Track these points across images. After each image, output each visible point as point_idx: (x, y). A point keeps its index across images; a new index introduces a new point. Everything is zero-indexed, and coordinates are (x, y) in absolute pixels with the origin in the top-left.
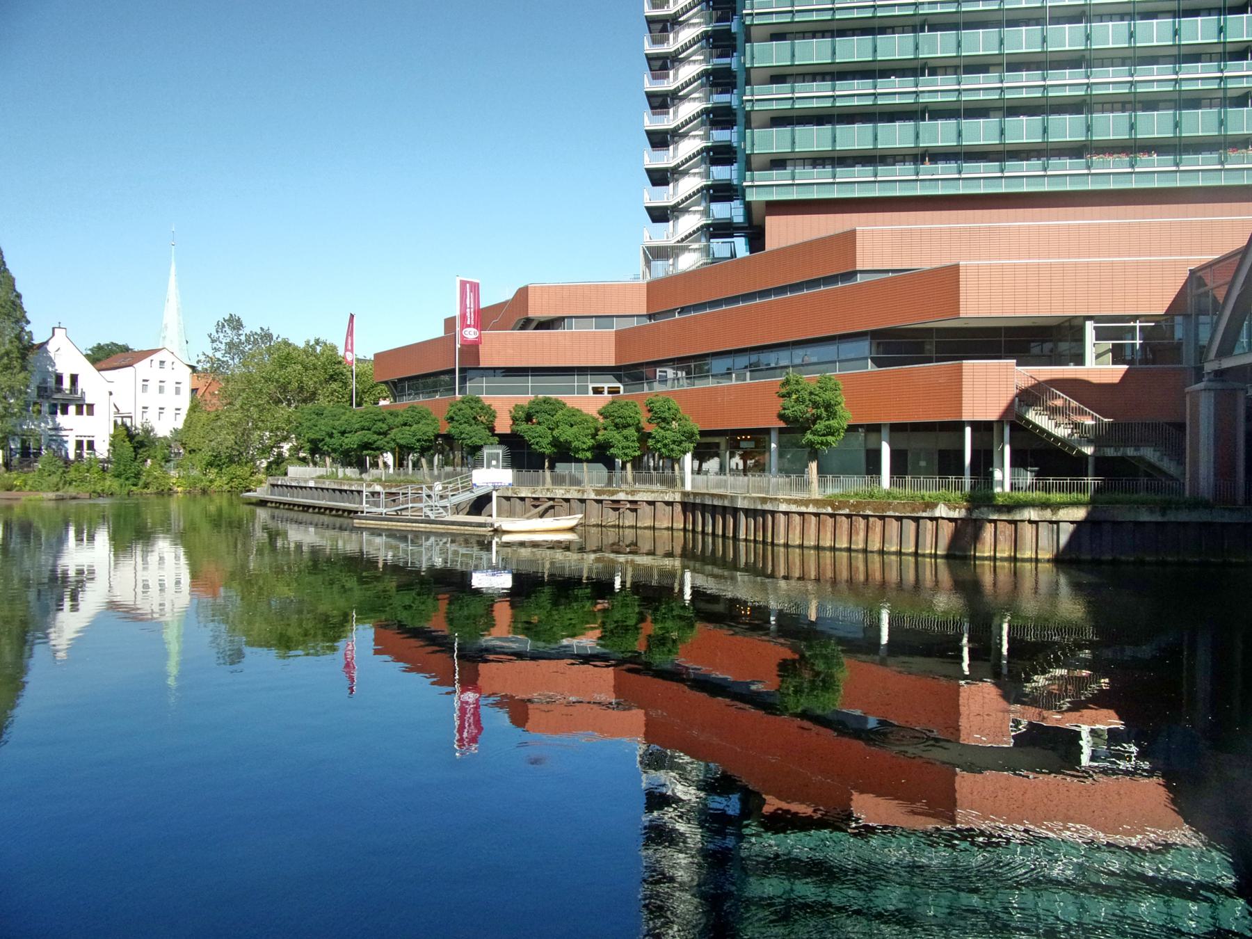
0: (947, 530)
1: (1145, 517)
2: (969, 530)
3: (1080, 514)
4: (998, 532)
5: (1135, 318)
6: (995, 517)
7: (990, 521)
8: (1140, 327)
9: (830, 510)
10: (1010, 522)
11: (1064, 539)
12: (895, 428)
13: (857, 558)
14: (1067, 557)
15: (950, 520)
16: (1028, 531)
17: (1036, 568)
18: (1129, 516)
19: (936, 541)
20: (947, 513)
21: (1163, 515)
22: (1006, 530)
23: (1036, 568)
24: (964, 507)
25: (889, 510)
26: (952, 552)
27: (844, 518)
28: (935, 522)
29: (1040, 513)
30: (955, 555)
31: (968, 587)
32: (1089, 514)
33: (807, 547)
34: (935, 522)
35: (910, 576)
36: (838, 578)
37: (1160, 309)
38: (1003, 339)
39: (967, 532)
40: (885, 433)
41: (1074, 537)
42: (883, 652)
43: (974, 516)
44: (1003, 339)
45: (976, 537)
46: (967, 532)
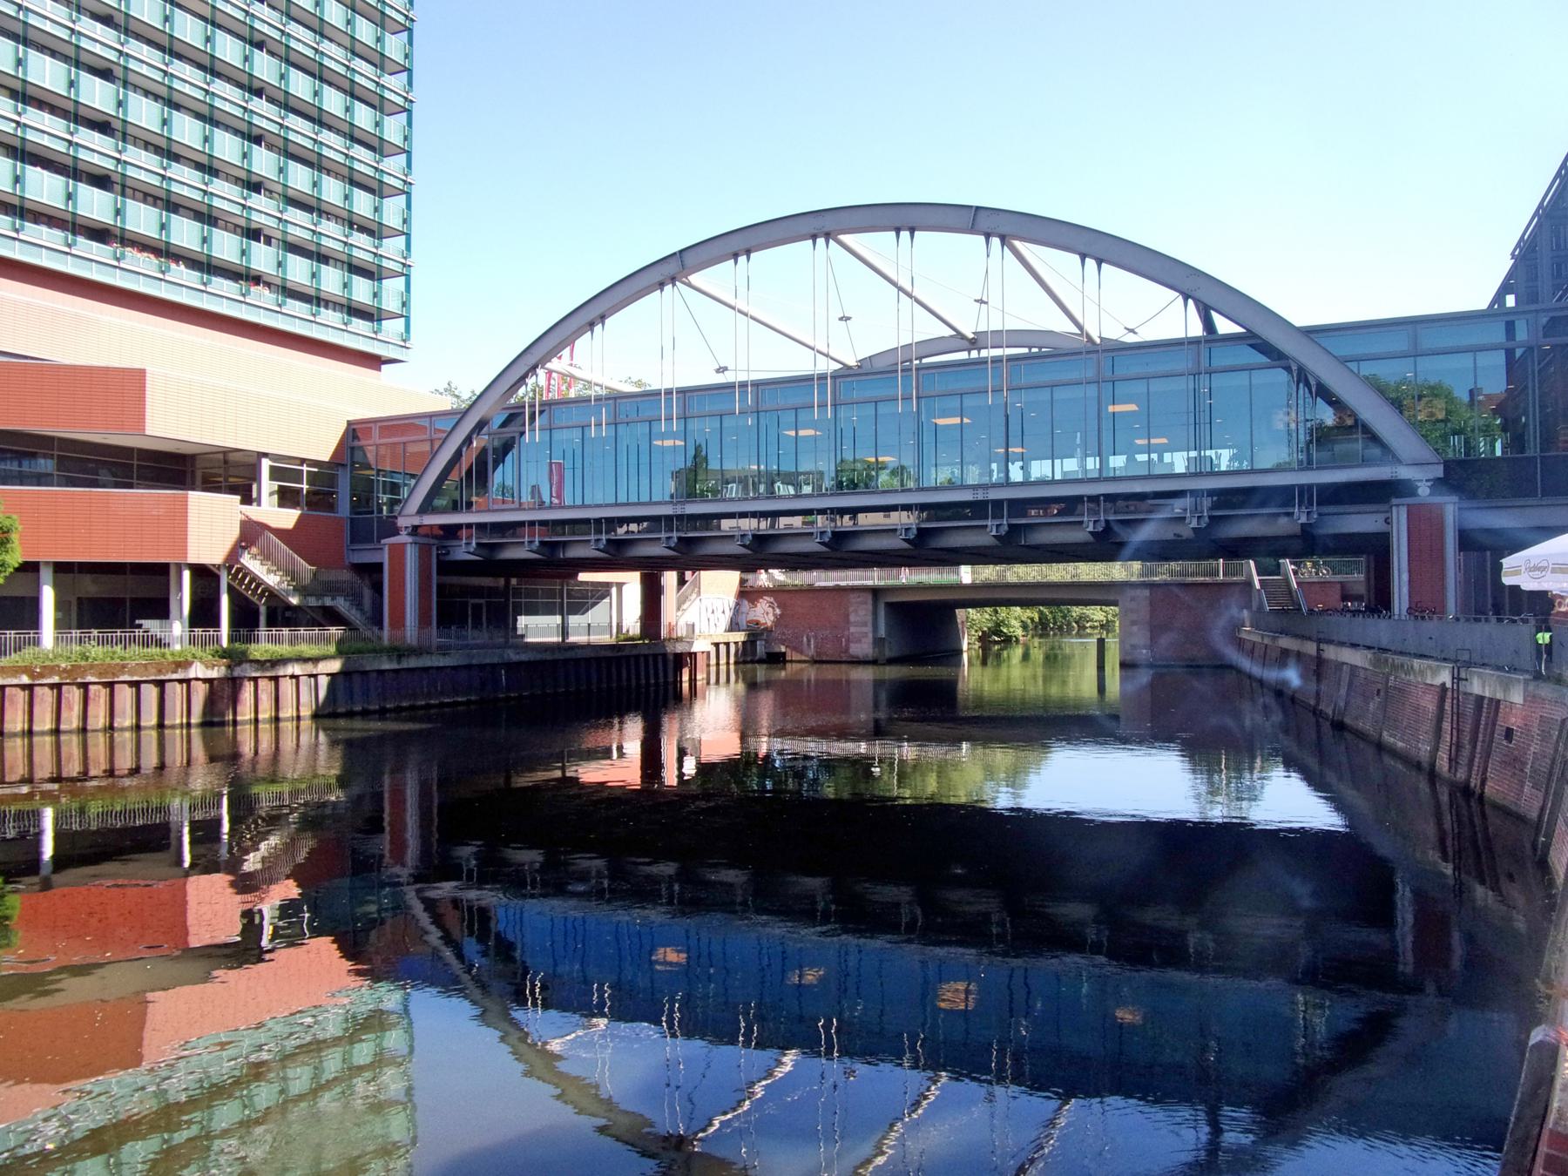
0: (200, 693)
1: (386, 666)
2: (227, 691)
3: (335, 666)
4: (260, 692)
5: (303, 461)
6: (254, 675)
7: (250, 679)
8: (308, 471)
9: (25, 680)
10: (271, 678)
11: (322, 694)
12: (61, 568)
13: (71, 741)
14: (326, 712)
15: (205, 681)
16: (287, 687)
17: (298, 728)
18: (376, 666)
19: (187, 707)
20: (204, 673)
21: (399, 662)
22: (266, 687)
23: (298, 728)
24: (224, 664)
25: (123, 674)
26: (208, 719)
27: (46, 689)
28: (185, 685)
29: (303, 666)
30: (401, 707)
31: (225, 756)
32: (344, 665)
33: (66, 732)
34: (185, 685)
35: (150, 760)
36: (168, 761)
37: (325, 455)
38: (135, 462)
39: (223, 695)
40: (46, 574)
41: (332, 687)
42: (46, 870)
43: (236, 674)
44: (135, 462)
45: (235, 701)
46: (223, 695)
